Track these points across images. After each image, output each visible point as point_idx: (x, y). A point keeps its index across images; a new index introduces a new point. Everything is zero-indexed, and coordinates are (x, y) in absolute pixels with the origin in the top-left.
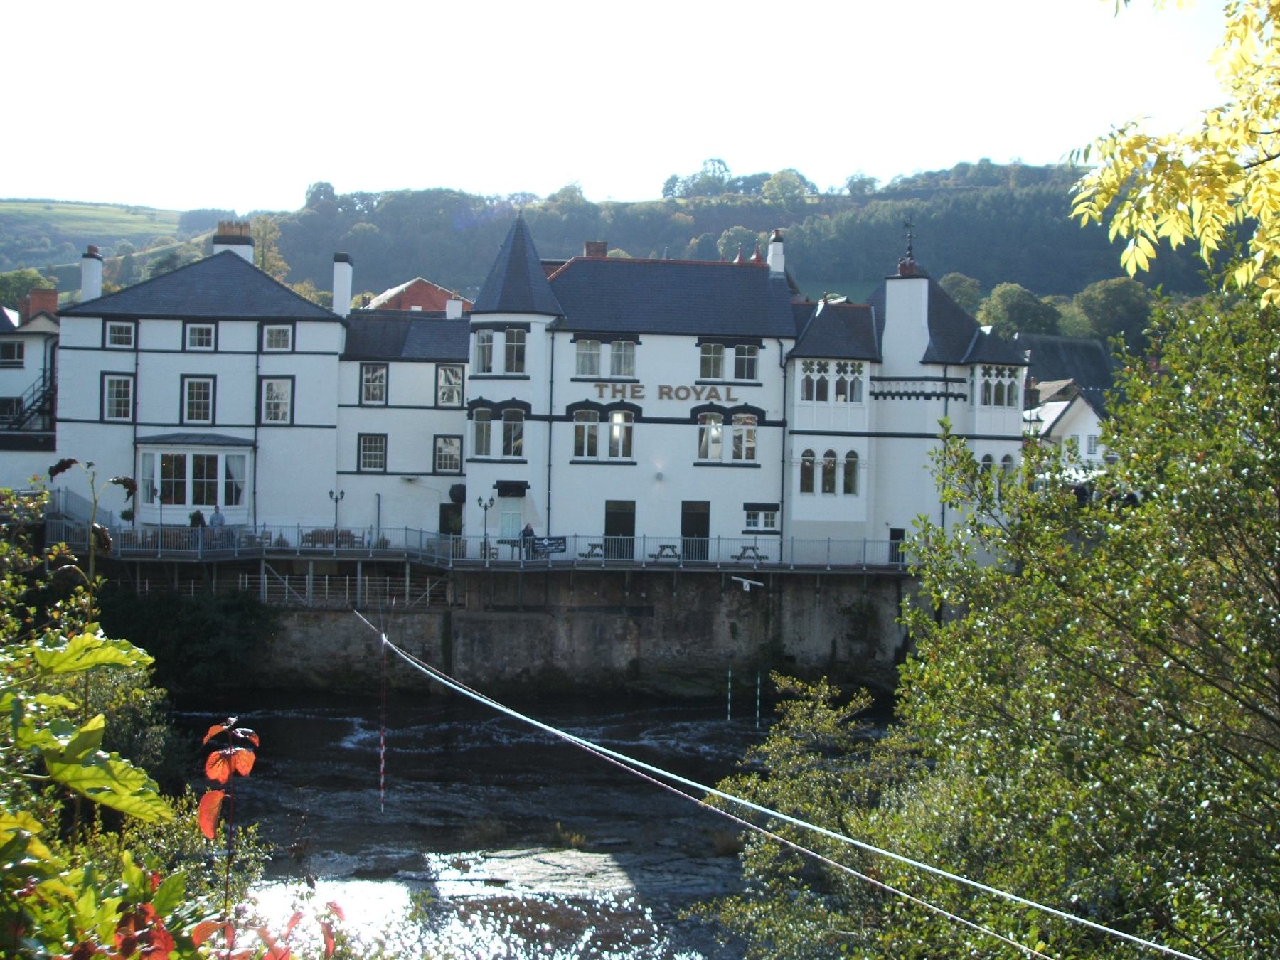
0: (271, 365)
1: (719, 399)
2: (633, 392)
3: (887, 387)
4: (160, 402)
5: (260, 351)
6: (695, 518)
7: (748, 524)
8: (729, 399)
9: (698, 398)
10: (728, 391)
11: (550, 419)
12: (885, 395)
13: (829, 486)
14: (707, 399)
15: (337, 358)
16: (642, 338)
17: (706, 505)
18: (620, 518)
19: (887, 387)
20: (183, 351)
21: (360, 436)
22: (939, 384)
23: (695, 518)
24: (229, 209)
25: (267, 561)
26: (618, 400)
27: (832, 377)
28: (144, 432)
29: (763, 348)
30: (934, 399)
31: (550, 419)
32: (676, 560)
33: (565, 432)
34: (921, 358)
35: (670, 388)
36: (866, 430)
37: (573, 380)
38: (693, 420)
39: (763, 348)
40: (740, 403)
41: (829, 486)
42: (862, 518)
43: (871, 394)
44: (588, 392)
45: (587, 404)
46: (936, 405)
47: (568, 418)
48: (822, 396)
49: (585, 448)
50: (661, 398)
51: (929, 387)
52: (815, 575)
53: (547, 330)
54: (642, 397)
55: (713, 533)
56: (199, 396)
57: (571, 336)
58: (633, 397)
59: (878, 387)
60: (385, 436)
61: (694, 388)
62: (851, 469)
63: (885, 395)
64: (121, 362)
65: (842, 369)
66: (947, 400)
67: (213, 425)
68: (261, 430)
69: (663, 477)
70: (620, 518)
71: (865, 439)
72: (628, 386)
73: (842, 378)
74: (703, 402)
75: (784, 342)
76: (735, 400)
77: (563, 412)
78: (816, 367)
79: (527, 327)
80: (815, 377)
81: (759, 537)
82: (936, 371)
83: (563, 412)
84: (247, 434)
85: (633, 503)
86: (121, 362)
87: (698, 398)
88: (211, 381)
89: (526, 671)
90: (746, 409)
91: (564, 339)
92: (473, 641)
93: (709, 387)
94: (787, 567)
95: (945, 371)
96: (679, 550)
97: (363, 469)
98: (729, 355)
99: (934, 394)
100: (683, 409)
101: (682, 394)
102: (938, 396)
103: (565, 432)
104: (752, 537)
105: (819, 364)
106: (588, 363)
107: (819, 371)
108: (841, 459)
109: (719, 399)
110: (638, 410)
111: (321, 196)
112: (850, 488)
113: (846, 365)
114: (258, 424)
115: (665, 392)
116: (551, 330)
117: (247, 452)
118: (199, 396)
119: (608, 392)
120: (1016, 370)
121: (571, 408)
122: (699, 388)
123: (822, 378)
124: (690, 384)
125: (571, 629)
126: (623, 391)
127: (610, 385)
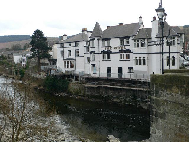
0: (77, 48)
3: (151, 44)
4: (66, 54)
5: (75, 46)
6: (120, 70)
8: (125, 48)
9: (120, 49)
11: (99, 54)
12: (151, 45)
13: (140, 64)
16: (111, 39)
17: (110, 68)
18: (109, 70)
20: (68, 47)
21: (87, 58)
22: (159, 42)
23: (120, 70)
28: (65, 58)
30: (157, 45)
31: (99, 54)
33: (101, 55)
36: (146, 53)
41: (140, 64)
42: (146, 70)
43: (178, 43)
44: (104, 49)
45: (104, 51)
48: (138, 47)
49: (104, 57)
51: (156, 43)
55: (112, 73)
56: (70, 52)
59: (149, 44)
60: (89, 57)
64: (62, 49)
70: (109, 70)
71: (146, 54)
74: (121, 49)
77: (101, 53)
78: (137, 41)
79: (94, 39)
80: (137, 43)
81: (131, 74)
83: (101, 53)
84: (74, 58)
86: (62, 49)
87: (120, 49)
91: (100, 41)
94: (135, 79)
98: (125, 40)
101: (117, 48)
102: (158, 45)
103: (101, 55)
104: (130, 73)
105: (137, 40)
106: (104, 44)
108: (142, 58)
109: (123, 49)
111: (42, 31)
112: (144, 64)
114: (76, 57)
118: (70, 52)
119: (106, 49)
122: (120, 47)
123: (144, 42)
124: (118, 46)
126: (109, 48)
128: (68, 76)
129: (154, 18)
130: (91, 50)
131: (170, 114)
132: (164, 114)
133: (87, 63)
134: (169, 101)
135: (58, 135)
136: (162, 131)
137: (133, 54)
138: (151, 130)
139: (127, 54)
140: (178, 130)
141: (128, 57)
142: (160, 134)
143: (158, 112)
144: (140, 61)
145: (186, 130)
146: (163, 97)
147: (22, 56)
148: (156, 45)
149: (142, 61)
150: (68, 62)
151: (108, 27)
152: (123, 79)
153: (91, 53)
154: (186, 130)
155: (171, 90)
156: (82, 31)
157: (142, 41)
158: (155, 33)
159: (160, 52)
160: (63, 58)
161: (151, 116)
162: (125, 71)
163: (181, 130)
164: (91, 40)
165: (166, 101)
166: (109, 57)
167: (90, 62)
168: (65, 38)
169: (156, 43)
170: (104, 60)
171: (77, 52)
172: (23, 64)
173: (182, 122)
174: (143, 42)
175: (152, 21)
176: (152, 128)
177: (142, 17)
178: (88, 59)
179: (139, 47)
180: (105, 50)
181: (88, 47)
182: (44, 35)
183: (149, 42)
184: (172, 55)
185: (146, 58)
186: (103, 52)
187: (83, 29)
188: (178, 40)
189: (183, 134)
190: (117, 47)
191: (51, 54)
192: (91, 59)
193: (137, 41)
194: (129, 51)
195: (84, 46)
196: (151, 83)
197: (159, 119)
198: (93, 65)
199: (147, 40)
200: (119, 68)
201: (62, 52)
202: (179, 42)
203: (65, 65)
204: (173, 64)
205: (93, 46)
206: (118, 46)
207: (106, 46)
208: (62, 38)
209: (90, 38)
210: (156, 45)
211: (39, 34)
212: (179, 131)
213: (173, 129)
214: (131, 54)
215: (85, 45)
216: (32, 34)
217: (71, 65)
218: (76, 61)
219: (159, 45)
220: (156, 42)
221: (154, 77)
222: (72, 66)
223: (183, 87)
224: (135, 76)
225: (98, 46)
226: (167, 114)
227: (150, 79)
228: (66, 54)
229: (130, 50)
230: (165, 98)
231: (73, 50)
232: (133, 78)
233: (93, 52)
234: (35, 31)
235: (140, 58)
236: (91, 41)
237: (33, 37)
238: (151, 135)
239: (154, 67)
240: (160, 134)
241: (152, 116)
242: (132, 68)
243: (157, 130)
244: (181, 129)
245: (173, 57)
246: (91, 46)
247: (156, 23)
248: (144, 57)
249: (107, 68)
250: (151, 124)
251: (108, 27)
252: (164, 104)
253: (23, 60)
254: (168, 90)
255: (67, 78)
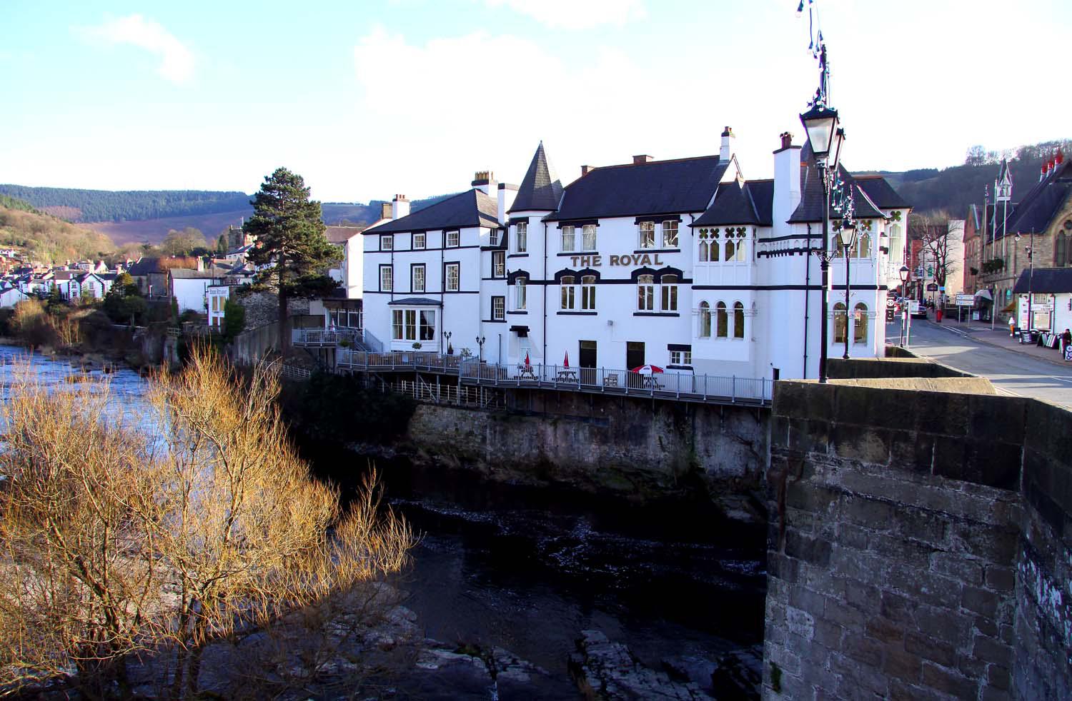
0: (450, 256)
1: (650, 264)
2: (594, 261)
3: (768, 247)
4: (402, 282)
5: (444, 248)
6: (635, 353)
7: (673, 361)
8: (657, 263)
9: (636, 264)
10: (656, 257)
11: (545, 283)
12: (768, 254)
13: (722, 332)
14: (642, 263)
15: (479, 249)
16: (600, 221)
17: (641, 345)
18: (588, 353)
19: (768, 247)
20: (412, 250)
21: (493, 298)
22: (801, 240)
23: (635, 353)
24: (933, 168)
25: (420, 374)
26: (584, 268)
27: (722, 241)
28: (397, 298)
29: (681, 221)
30: (797, 254)
31: (545, 283)
32: (575, 383)
34: (789, 219)
35: (617, 257)
37: (558, 255)
38: (633, 280)
39: (681, 221)
40: (665, 266)
41: (722, 332)
44: (567, 263)
45: (567, 272)
46: (800, 259)
47: (556, 282)
48: (715, 258)
49: (567, 300)
50: (612, 264)
51: (792, 244)
52: (719, 406)
53: (542, 221)
54: (600, 265)
56: (419, 269)
57: (557, 224)
58: (594, 265)
59: (761, 247)
61: (633, 256)
62: (739, 316)
63: (768, 254)
64: (386, 258)
65: (729, 233)
66: (809, 254)
67: (425, 293)
68: (445, 295)
69: (616, 321)
70: (588, 353)
71: (748, 292)
72: (591, 257)
73: (730, 241)
74: (640, 267)
75: (693, 214)
76: (661, 264)
78: (709, 234)
79: (526, 220)
80: (709, 241)
81: (681, 372)
82: (802, 229)
84: (438, 298)
85: (580, 342)
86: (386, 258)
87: (636, 264)
88: (382, 267)
89: (528, 456)
90: (669, 270)
92: (495, 432)
93: (643, 255)
94: (700, 397)
95: (809, 228)
96: (577, 376)
97: (495, 319)
99: (797, 250)
100: (626, 273)
101: (626, 261)
102: (801, 251)
103: (555, 291)
104: (676, 371)
105: (712, 231)
107: (712, 237)
108: (730, 308)
109: (650, 264)
110: (598, 274)
112: (739, 333)
113: (733, 230)
114: (444, 292)
115: (614, 260)
116: (545, 221)
117: (436, 309)
118: (419, 269)
119: (579, 262)
120: (870, 222)
121: (558, 275)
122: (636, 255)
123: (714, 242)
125: (555, 430)
126: (588, 261)
127: (580, 257)
128: (410, 376)
129: (786, 139)
130: (512, 265)
131: (850, 544)
132: (826, 547)
133: (492, 320)
134: (848, 494)
135: (181, 409)
136: (815, 614)
137: (694, 288)
138: (768, 611)
139: (665, 290)
140: (879, 609)
141: (670, 302)
142: (806, 627)
143: (800, 538)
144: (723, 317)
145: (910, 612)
146: (823, 474)
147: (209, 282)
148: (791, 252)
149: (729, 322)
150: (411, 315)
151: (584, 168)
152: (599, 388)
153: (511, 279)
154: (910, 612)
155: (855, 447)
156: (474, 183)
157: (733, 236)
158: (787, 201)
159: (810, 291)
160: (388, 298)
161: (771, 554)
162: (656, 356)
163: (888, 609)
164: (513, 222)
165: (835, 491)
166: (589, 300)
167: (507, 317)
168: (403, 211)
169: (792, 247)
170: (568, 310)
171: (451, 273)
172: (215, 319)
173: (896, 579)
174: (735, 240)
175: (775, 152)
176: (771, 602)
177: (723, 131)
178: (497, 302)
179: (717, 260)
180: (571, 268)
181: (498, 250)
182: (309, 195)
183: (761, 240)
184: (856, 297)
185: (747, 308)
186: (562, 276)
187: (477, 175)
188: (882, 234)
189: (898, 626)
190: (623, 257)
191: (337, 279)
192: (511, 305)
193: (709, 234)
194: (675, 275)
195: (484, 249)
196: (775, 415)
197: (803, 565)
198: (521, 331)
199: (754, 231)
200: (690, 346)
201: (388, 269)
202: (886, 245)
203: (395, 327)
204: (861, 337)
205: (520, 250)
206: (630, 253)
207: (577, 250)
208: (377, 209)
209: (508, 213)
210: (791, 252)
211: (282, 188)
212: (884, 613)
213: (858, 607)
214: (681, 288)
215: (488, 244)
216: (258, 189)
217: (423, 330)
218: (444, 312)
219: (805, 254)
220: (792, 241)
221: (789, 395)
222: (427, 333)
223: (906, 438)
224: (699, 381)
225: (544, 246)
226: (835, 545)
227: (769, 395)
228: (402, 282)
229: (680, 273)
230: (831, 480)
231: (433, 261)
232: (689, 391)
233: (520, 277)
234: (270, 176)
235: (721, 304)
236: (513, 230)
237: (261, 199)
238: (766, 631)
239: (777, 350)
240: (806, 627)
241: (773, 552)
242: (687, 348)
243: (790, 611)
244: (890, 604)
245: (861, 306)
246: (512, 248)
247: (794, 157)
248: (738, 304)
249: (625, 346)
250: (770, 586)
251: (584, 168)
252: (823, 505)
253: (215, 299)
254: (846, 448)
255: (404, 384)
